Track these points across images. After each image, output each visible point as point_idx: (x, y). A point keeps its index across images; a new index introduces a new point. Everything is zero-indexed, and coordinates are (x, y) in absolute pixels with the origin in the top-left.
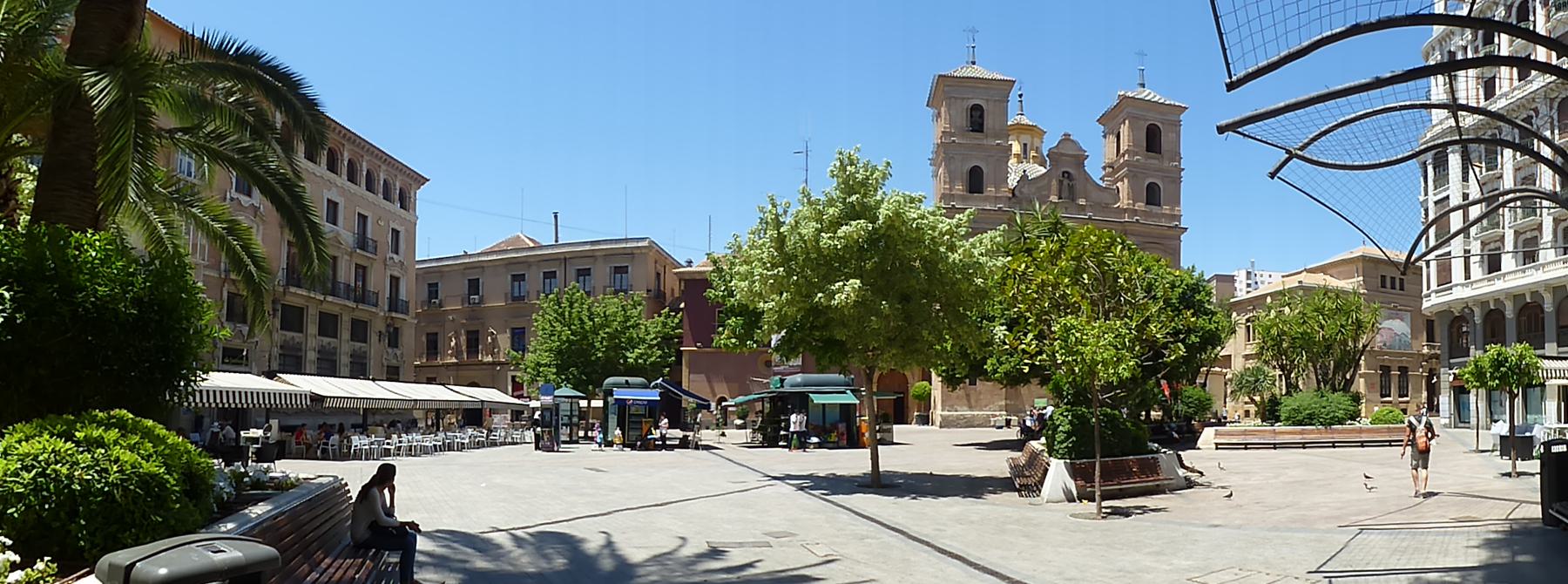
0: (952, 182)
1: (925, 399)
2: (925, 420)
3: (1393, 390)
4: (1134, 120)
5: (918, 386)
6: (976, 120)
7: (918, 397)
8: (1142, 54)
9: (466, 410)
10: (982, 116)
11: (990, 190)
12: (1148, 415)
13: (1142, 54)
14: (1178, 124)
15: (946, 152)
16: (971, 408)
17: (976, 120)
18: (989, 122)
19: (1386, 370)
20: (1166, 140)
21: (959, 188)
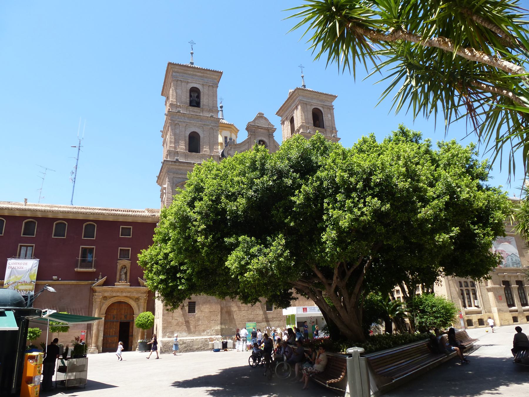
0: (176, 142)
1: (148, 327)
2: (150, 346)
3: (517, 301)
4: (304, 105)
5: (141, 316)
6: (195, 99)
7: (142, 326)
8: (301, 67)
9: (86, 346)
10: (198, 97)
11: (205, 150)
12: (388, 328)
13: (301, 67)
14: (331, 108)
15: (173, 119)
16: (189, 331)
17: (195, 99)
18: (204, 100)
19: (507, 284)
20: (326, 118)
21: (182, 147)
